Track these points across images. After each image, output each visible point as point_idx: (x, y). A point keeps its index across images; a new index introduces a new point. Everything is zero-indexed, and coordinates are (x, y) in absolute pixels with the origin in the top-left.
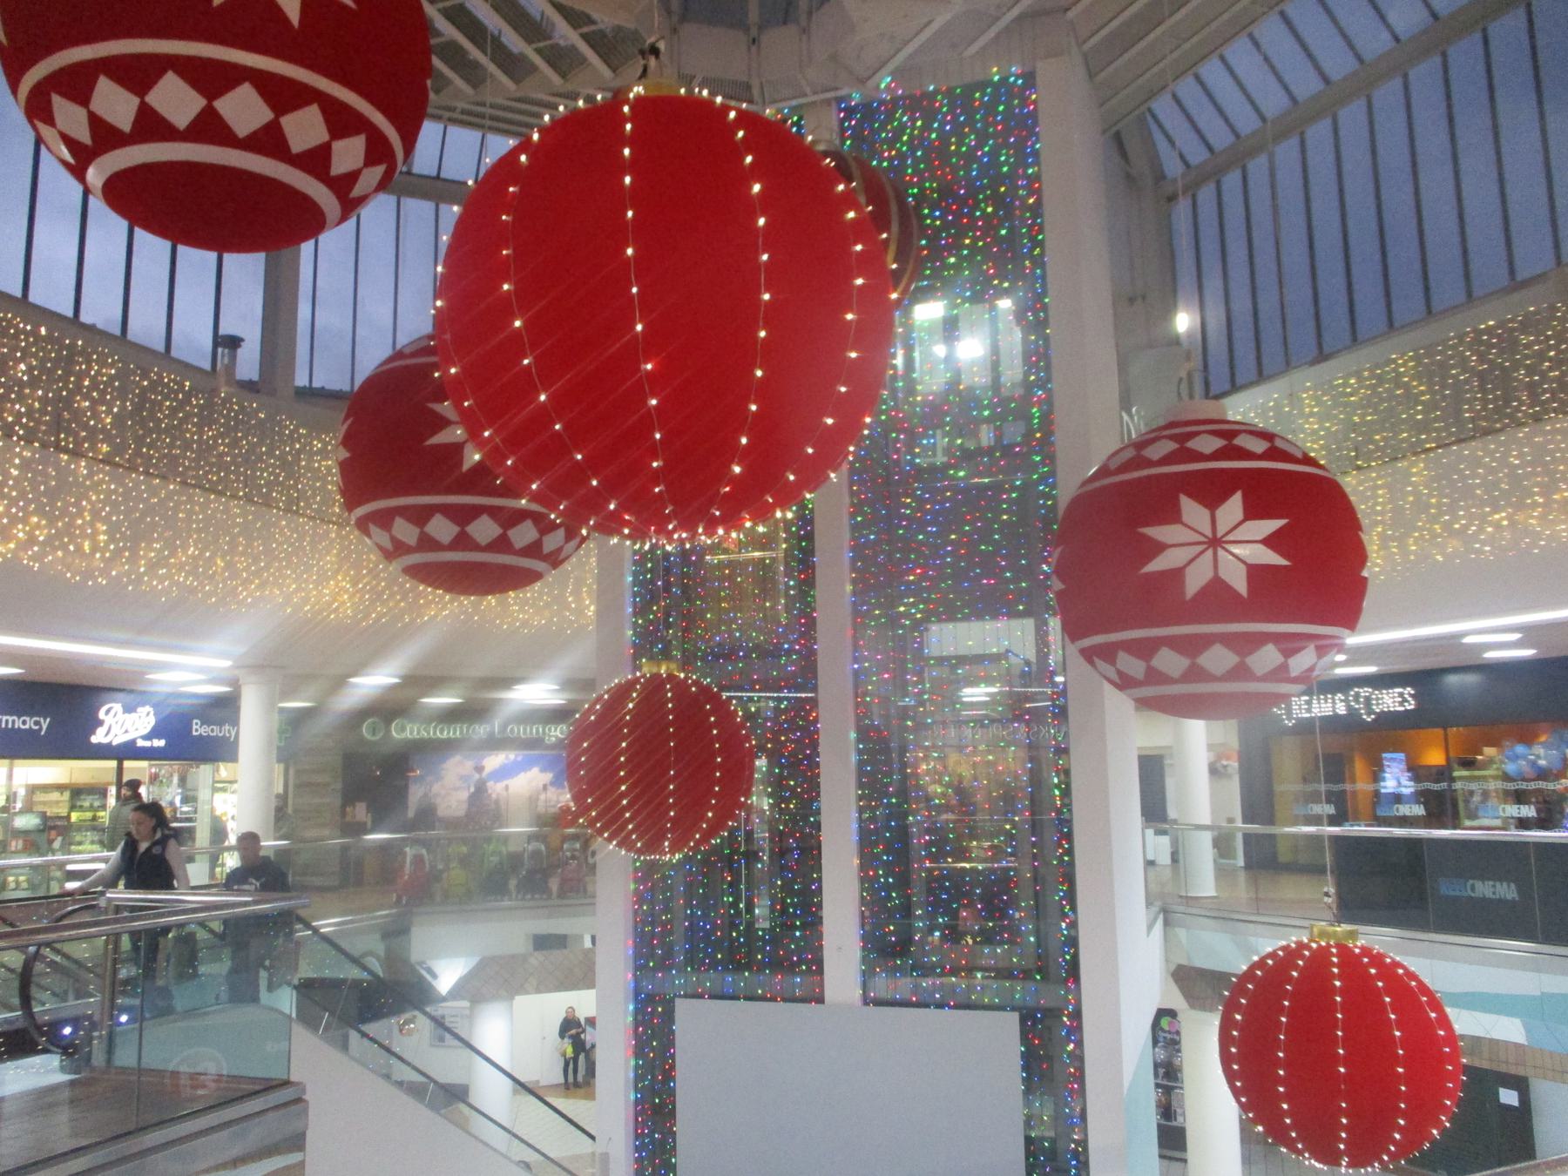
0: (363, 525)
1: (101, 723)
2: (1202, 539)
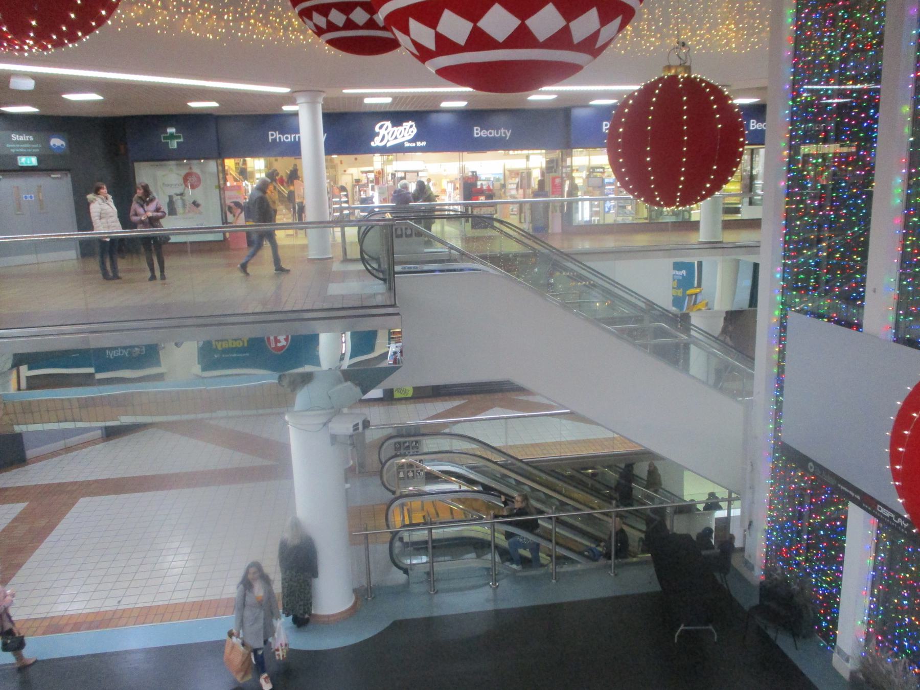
1: (378, 134)
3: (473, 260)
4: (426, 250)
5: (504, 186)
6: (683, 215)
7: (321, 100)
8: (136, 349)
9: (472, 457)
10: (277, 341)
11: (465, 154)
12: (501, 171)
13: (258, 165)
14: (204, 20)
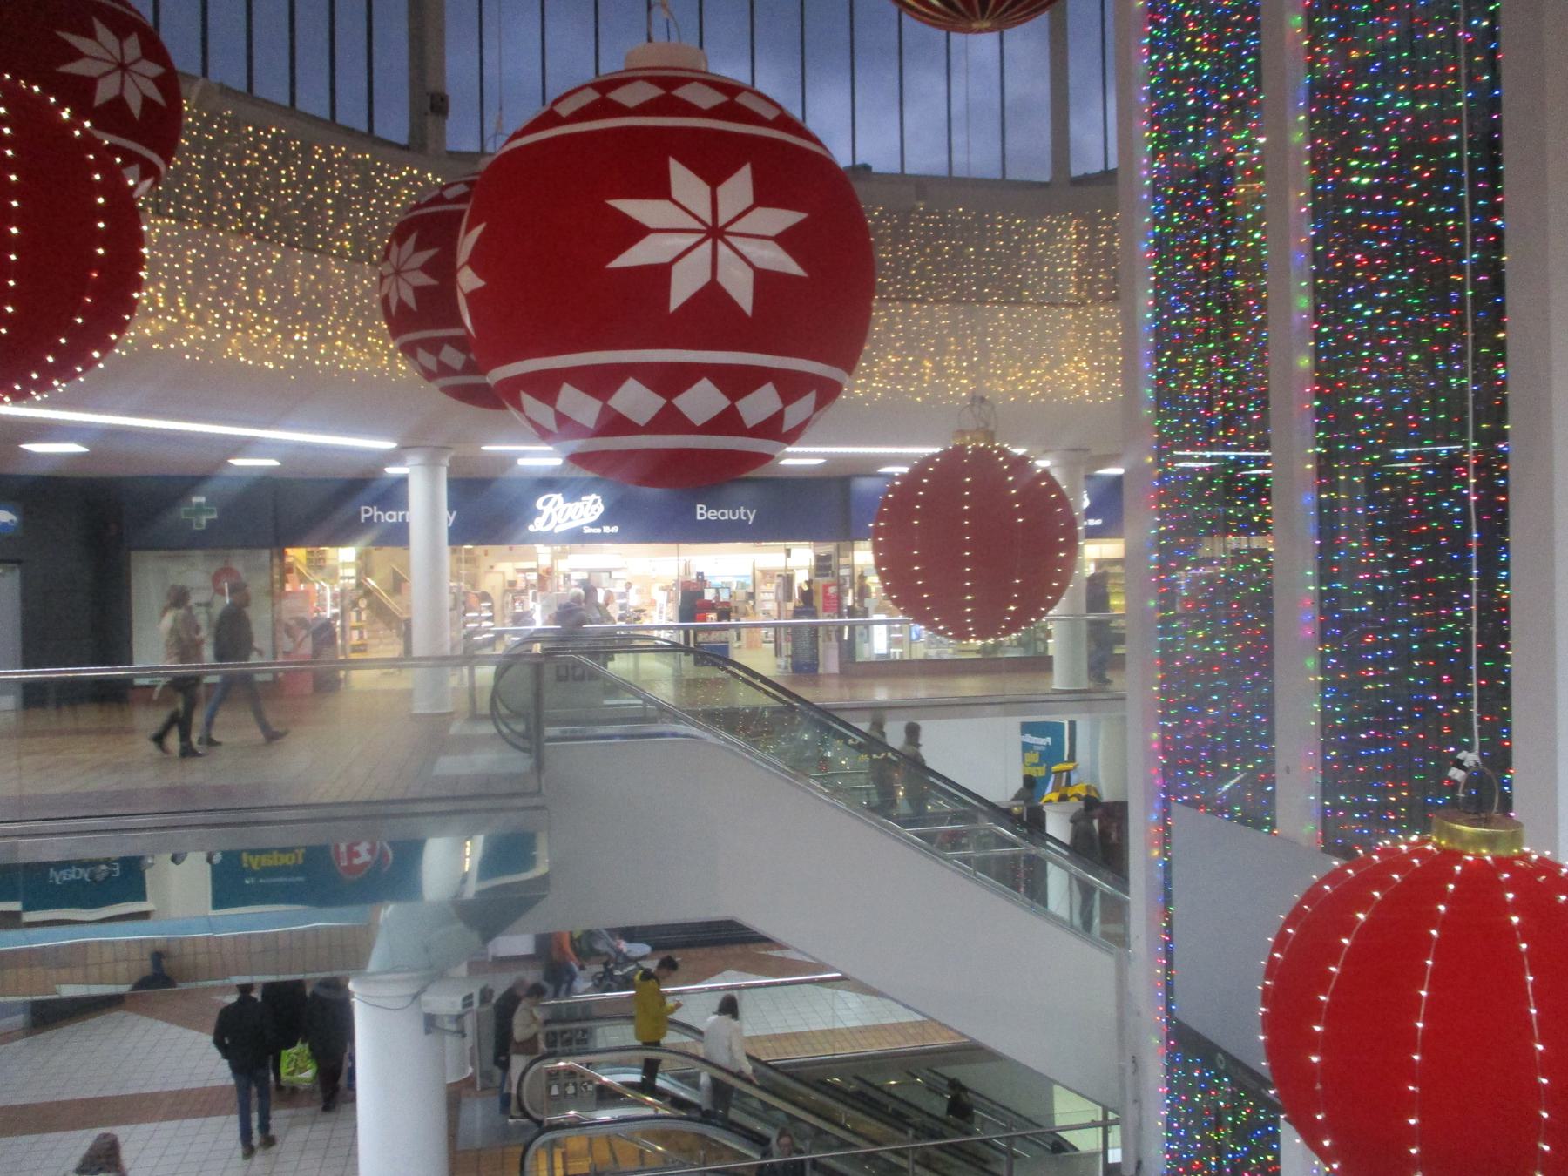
0: (409, 350)
1: (539, 513)
2: (702, 228)
3: (676, 719)
4: (607, 702)
5: (752, 596)
6: (1036, 647)
7: (446, 461)
8: (104, 867)
9: (680, 1058)
10: (352, 854)
11: (684, 546)
12: (750, 572)
14: (261, 341)
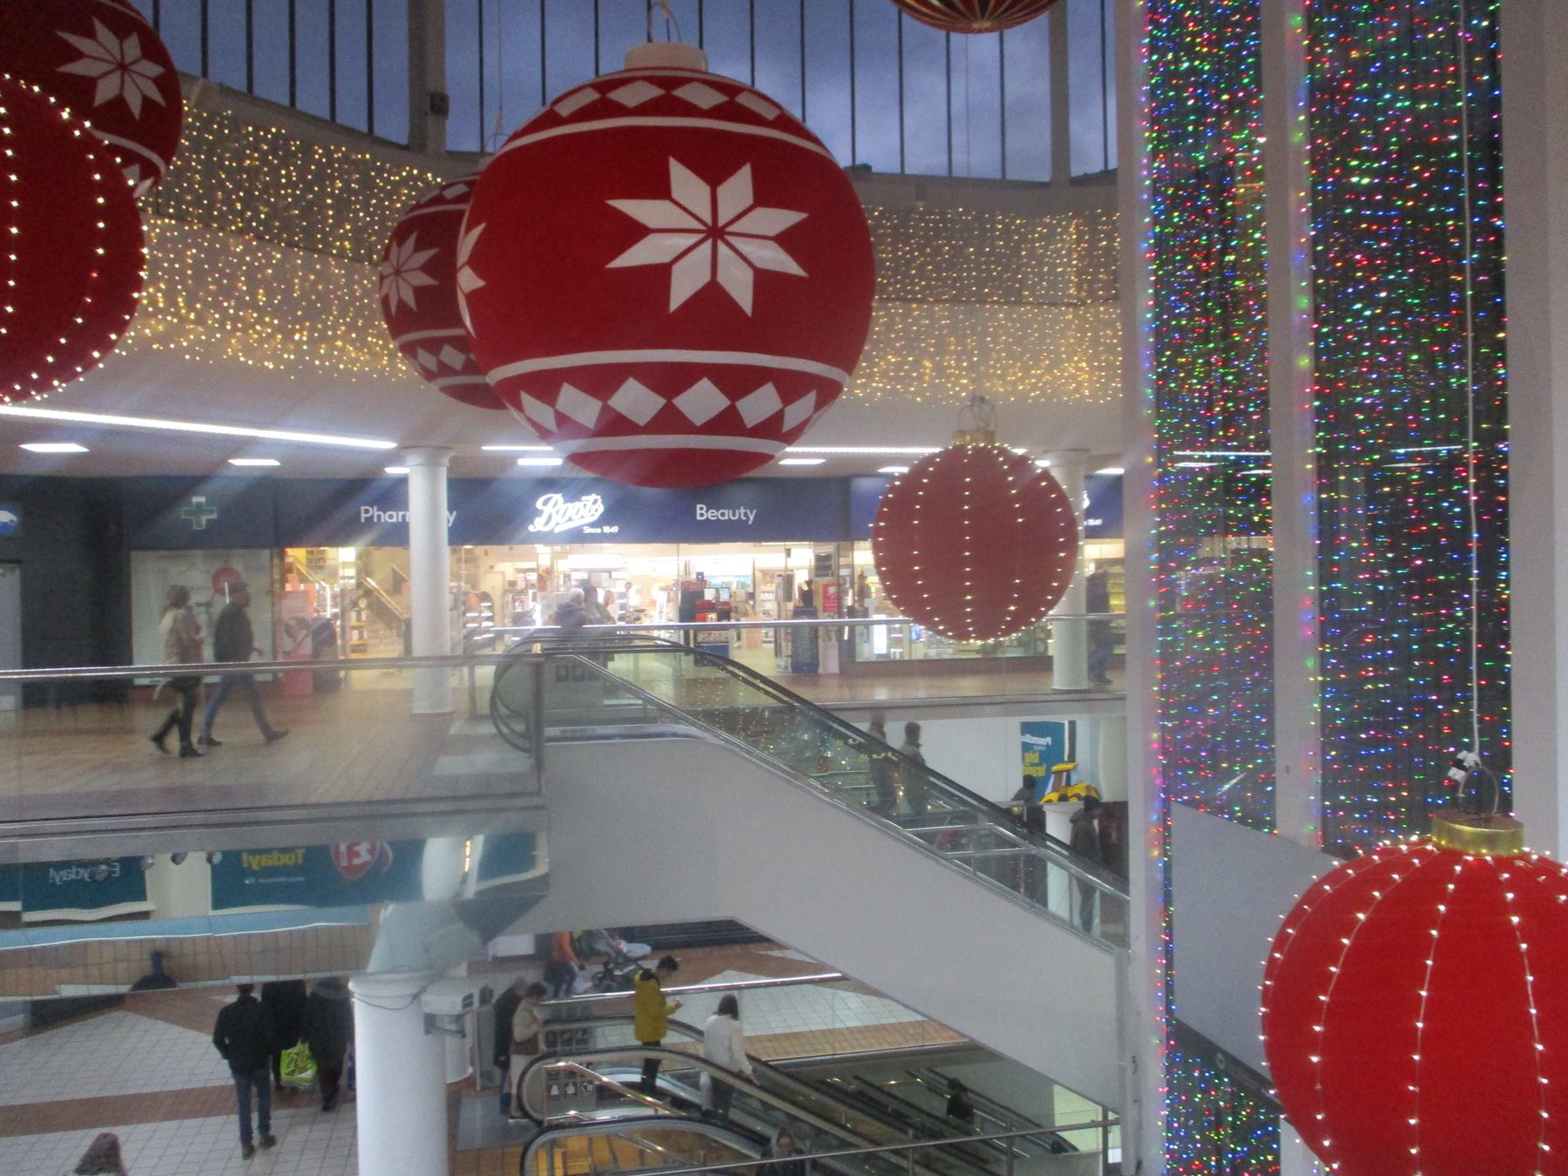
0: (409, 350)
1: (539, 513)
2: (702, 228)
3: (676, 719)
4: (607, 702)
5: (752, 596)
6: (1036, 647)
7: (446, 461)
8: (104, 867)
9: (680, 1058)
11: (684, 546)
12: (750, 572)
13: (344, 556)
14: (261, 341)
